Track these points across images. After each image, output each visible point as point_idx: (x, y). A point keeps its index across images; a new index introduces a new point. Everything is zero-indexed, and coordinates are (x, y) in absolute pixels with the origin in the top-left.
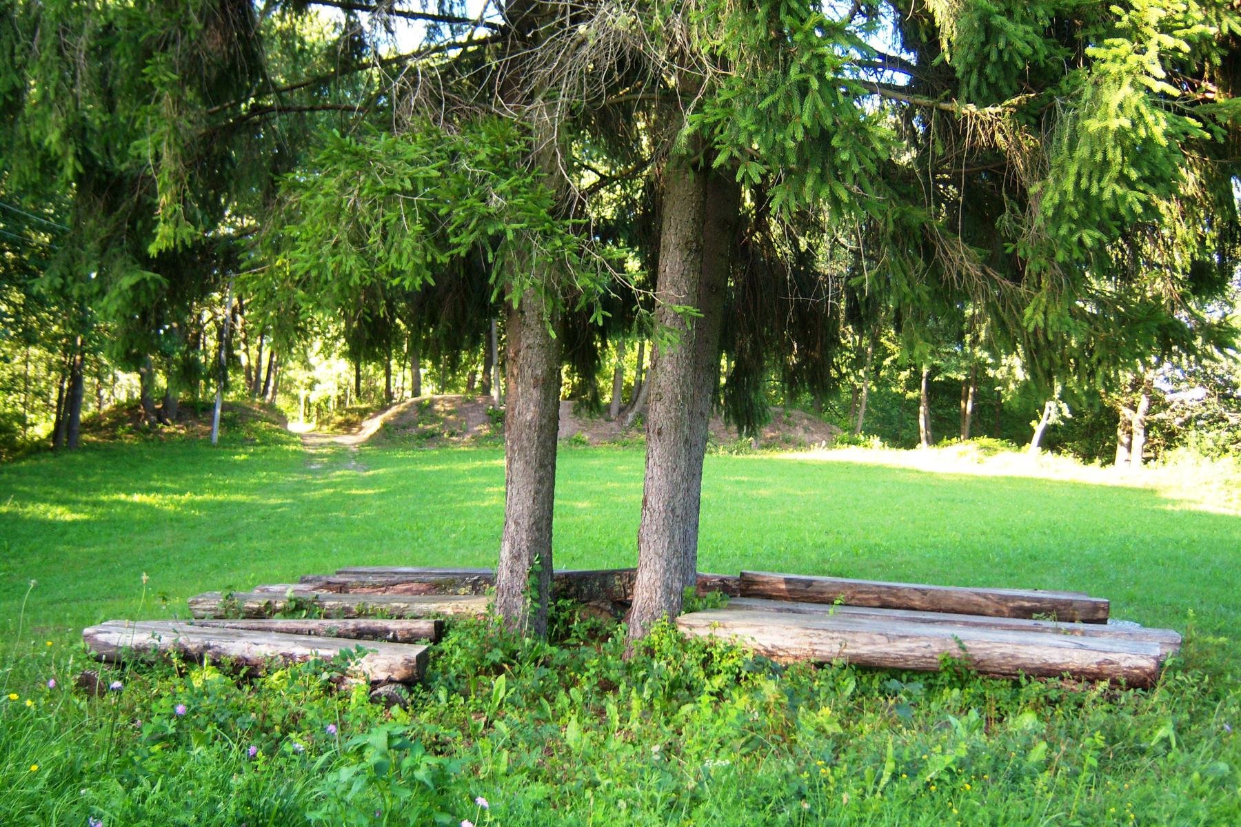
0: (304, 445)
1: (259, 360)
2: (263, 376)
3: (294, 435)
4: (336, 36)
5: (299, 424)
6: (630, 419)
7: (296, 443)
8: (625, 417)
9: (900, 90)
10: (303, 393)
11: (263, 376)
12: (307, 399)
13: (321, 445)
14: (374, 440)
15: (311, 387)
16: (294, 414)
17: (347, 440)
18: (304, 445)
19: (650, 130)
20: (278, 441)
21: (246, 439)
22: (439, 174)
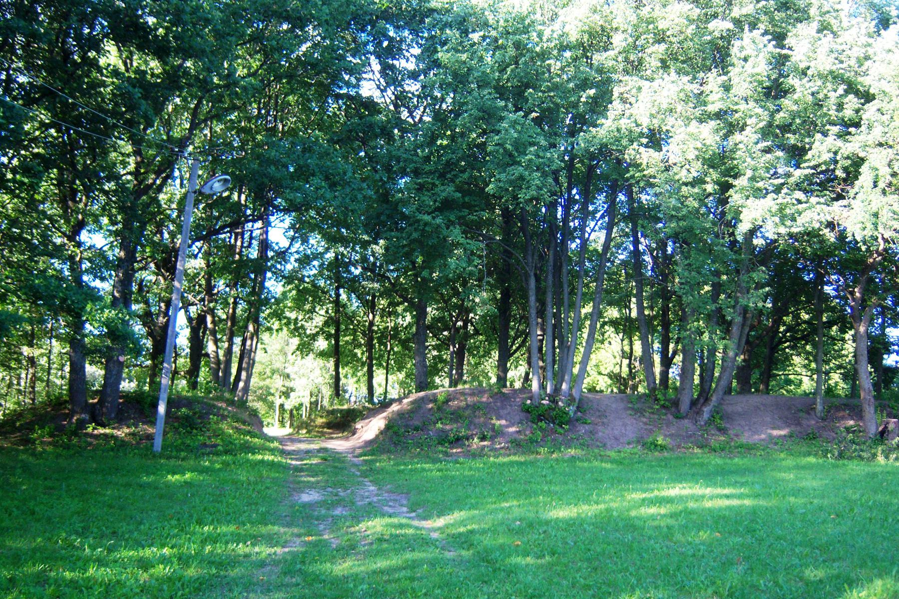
0: (283, 453)
1: (229, 352)
2: (234, 371)
3: (272, 439)
4: (812, 579)
5: (274, 429)
6: (706, 416)
7: (272, 451)
8: (699, 413)
9: (504, 306)
10: (278, 402)
11: (234, 371)
12: (282, 406)
13: (308, 452)
14: (374, 447)
15: (286, 394)
16: (269, 420)
17: (339, 444)
18: (283, 453)
19: (498, 419)
20: (248, 448)
21: (205, 445)
22: (844, 175)
